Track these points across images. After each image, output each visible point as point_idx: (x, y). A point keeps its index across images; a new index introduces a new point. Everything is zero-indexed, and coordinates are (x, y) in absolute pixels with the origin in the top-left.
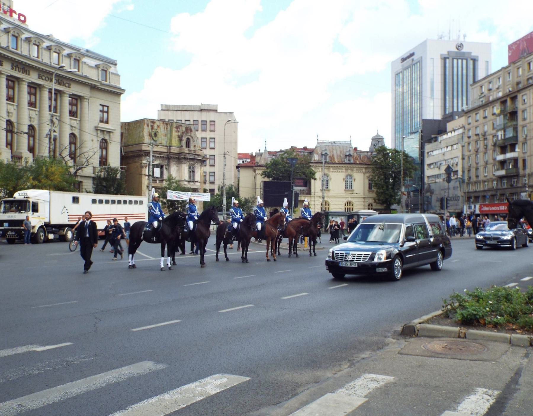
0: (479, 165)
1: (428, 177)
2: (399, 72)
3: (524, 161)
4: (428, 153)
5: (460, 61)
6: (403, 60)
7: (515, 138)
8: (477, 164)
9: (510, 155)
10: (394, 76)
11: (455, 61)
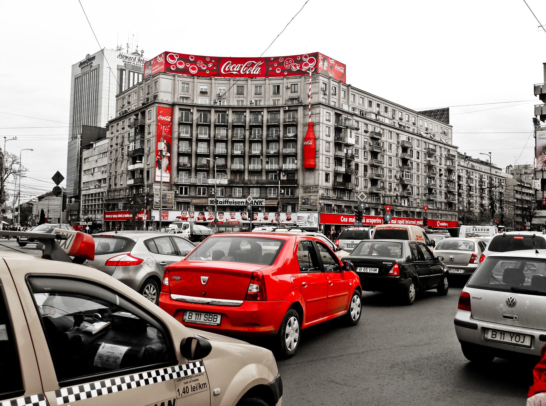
0: (118, 173)
1: (84, 183)
2: (78, 76)
3: (148, 172)
4: (85, 159)
5: (136, 75)
6: (81, 64)
7: (142, 150)
8: (116, 172)
9: (138, 166)
10: (74, 79)
11: (132, 74)
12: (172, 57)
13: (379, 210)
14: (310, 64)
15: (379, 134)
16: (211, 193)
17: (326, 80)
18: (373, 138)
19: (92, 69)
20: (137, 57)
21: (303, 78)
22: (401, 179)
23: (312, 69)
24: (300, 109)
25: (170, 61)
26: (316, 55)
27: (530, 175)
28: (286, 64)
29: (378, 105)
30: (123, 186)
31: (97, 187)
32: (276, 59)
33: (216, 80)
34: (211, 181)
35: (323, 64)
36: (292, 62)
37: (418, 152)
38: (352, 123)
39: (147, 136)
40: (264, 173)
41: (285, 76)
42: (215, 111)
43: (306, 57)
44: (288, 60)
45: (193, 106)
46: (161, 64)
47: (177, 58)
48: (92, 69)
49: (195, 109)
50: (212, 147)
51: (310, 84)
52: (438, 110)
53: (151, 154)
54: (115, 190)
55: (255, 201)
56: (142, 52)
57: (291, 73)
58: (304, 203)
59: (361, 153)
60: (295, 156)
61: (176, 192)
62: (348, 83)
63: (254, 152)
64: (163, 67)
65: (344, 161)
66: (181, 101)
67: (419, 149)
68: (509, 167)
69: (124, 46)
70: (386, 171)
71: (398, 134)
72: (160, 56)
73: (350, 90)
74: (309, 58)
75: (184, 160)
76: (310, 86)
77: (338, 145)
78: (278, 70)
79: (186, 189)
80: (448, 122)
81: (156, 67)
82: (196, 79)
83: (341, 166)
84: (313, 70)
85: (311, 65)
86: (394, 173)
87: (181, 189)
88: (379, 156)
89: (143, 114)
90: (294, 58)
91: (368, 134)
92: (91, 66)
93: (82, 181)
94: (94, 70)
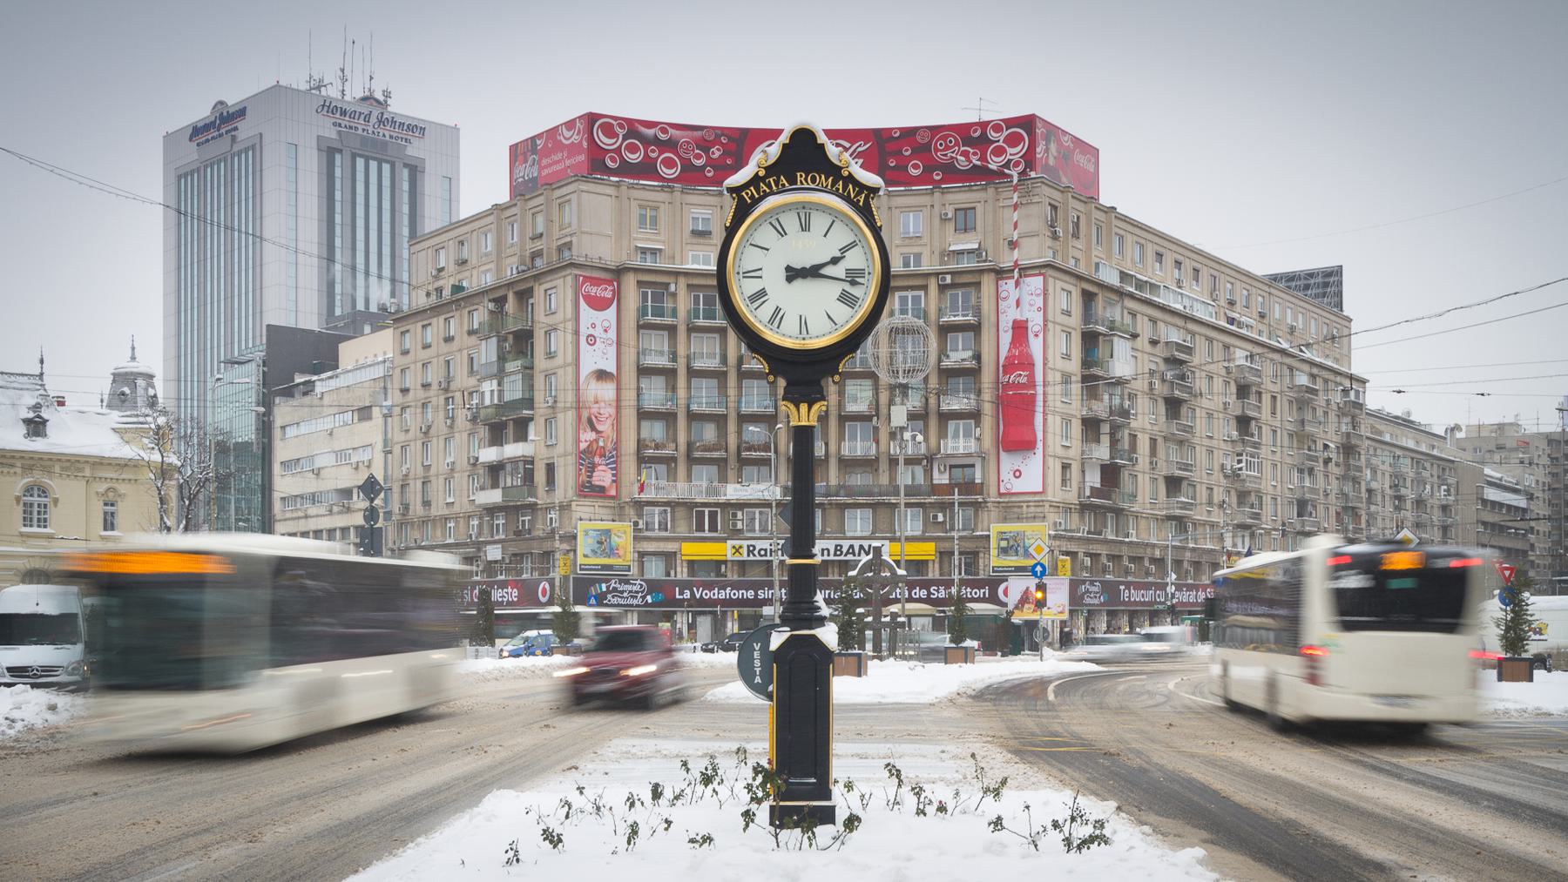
0: (433, 470)
1: (283, 499)
2: (188, 169)
3: (550, 469)
5: (373, 165)
6: (197, 131)
9: (512, 450)
10: (173, 180)
11: (360, 163)
12: (608, 131)
13: (1186, 564)
14: (1010, 151)
15: (1189, 350)
16: (735, 525)
17: (1057, 195)
18: (1172, 361)
19: (236, 148)
20: (375, 113)
21: (991, 191)
22: (1235, 475)
23: (1017, 164)
24: (987, 282)
25: (604, 141)
26: (1028, 122)
27: (1514, 455)
28: (937, 150)
29: (1178, 264)
30: (456, 509)
31: (335, 509)
32: (909, 133)
33: (631, 187)
34: (733, 492)
35: (1047, 150)
36: (957, 144)
37: (1274, 398)
38: (1116, 313)
39: (540, 362)
40: (884, 466)
41: (937, 184)
42: (688, 286)
43: (997, 128)
44: (944, 138)
45: (676, 274)
46: (573, 149)
47: (621, 132)
48: (236, 148)
49: (682, 282)
50: (682, 392)
51: (1015, 207)
52: (1311, 275)
53: (560, 416)
54: (424, 522)
55: (861, 547)
56: (387, 94)
57: (952, 173)
58: (1004, 551)
59: (1143, 404)
60: (975, 416)
61: (636, 524)
62: (1105, 199)
63: (852, 408)
64: (582, 158)
65: (1105, 428)
66: (637, 262)
67: (1276, 388)
68: (1452, 430)
69: (331, 76)
70: (1201, 453)
71: (1227, 347)
72: (570, 125)
73: (1115, 222)
74: (1006, 133)
75: (656, 431)
76: (1016, 216)
77: (1092, 382)
78: (916, 167)
79: (713, 516)
80: (1340, 305)
81: (555, 158)
82: (677, 194)
83: (1098, 441)
84: (1021, 168)
85: (1015, 153)
86: (1219, 458)
87: (701, 515)
88: (1184, 410)
89: (524, 295)
90: (962, 130)
91: (1158, 350)
92: (234, 138)
93: (277, 496)
94: (246, 150)
